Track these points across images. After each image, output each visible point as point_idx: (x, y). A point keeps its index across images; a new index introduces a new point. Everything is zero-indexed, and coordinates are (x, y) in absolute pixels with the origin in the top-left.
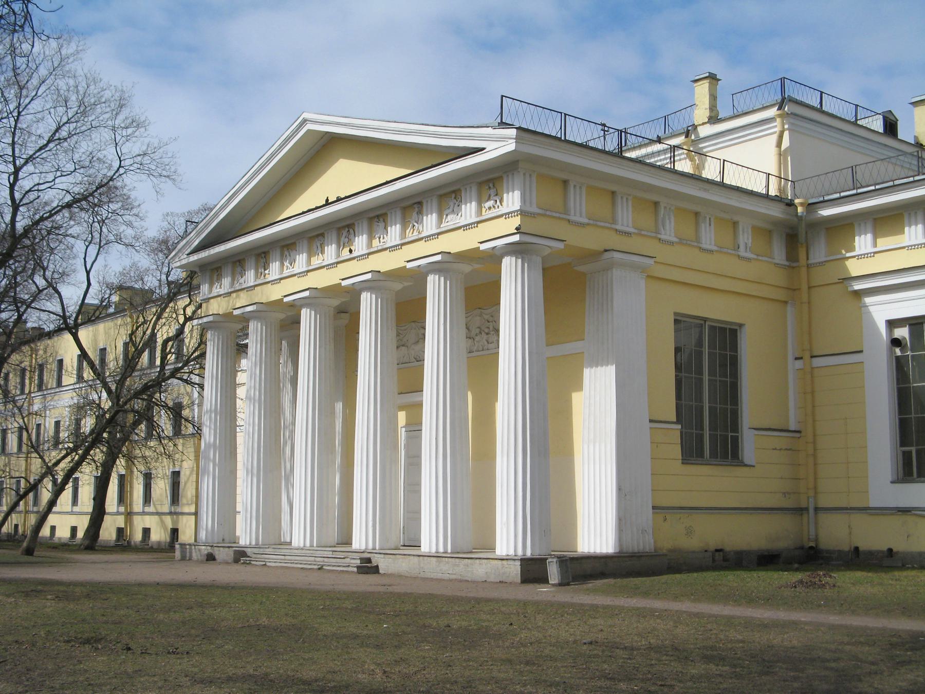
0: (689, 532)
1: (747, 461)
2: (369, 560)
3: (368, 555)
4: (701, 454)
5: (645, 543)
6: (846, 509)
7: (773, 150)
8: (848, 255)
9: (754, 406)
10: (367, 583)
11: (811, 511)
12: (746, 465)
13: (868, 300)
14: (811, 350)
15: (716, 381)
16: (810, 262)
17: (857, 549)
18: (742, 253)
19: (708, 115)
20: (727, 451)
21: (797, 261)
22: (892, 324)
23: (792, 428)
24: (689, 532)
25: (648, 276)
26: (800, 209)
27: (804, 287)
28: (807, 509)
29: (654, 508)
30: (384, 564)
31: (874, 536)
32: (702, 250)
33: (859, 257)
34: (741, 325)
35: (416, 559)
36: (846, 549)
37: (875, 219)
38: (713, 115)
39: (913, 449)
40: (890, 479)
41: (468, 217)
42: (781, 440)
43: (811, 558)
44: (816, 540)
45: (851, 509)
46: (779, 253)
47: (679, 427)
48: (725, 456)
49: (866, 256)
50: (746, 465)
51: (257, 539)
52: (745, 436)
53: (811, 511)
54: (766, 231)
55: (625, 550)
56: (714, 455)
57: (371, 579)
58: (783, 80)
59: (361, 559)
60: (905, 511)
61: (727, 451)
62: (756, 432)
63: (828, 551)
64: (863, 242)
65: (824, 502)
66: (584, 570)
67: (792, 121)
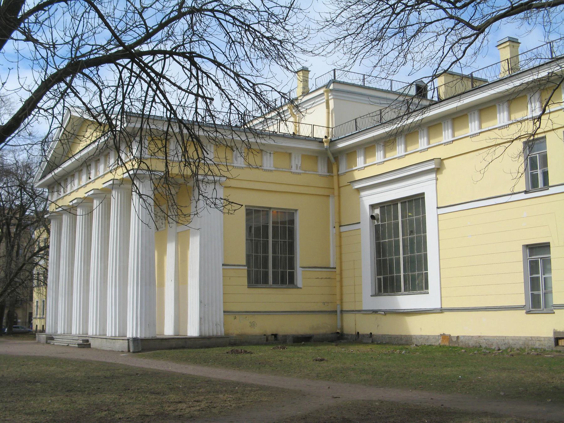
0: (253, 325)
1: (299, 286)
2: (87, 341)
3: (87, 338)
4: (266, 281)
5: (220, 331)
6: (353, 311)
7: (325, 110)
8: (354, 168)
9: (304, 253)
10: (84, 354)
11: (338, 312)
12: (298, 288)
13: (363, 194)
14: (340, 222)
15: (286, 242)
16: (339, 173)
17: (371, 333)
18: (294, 170)
19: (302, 91)
20: (286, 278)
21: (332, 172)
22: (373, 207)
23: (332, 266)
24: (253, 325)
25: (226, 187)
26: (325, 144)
27: (336, 187)
28: (336, 311)
29: (224, 312)
30: (94, 343)
31: (365, 326)
32: (265, 170)
33: (359, 169)
34: (296, 210)
35: (122, 341)
36: (354, 333)
37: (366, 148)
38: (305, 91)
39: (382, 277)
40: (371, 294)
41: (473, 130)
42: (324, 273)
43: (339, 337)
44: (342, 328)
45: (356, 311)
46: (322, 169)
47: (246, 268)
48: (283, 282)
49: (365, 168)
50: (298, 288)
51: (64, 331)
52: (298, 272)
53: (338, 312)
54: (314, 157)
55: (203, 335)
56: (275, 282)
57: (84, 351)
58: (334, 70)
59: (83, 340)
60: (375, 312)
61: (286, 278)
62: (304, 269)
63: (348, 335)
64: (360, 161)
65: (345, 308)
66: (180, 345)
67: (334, 93)
